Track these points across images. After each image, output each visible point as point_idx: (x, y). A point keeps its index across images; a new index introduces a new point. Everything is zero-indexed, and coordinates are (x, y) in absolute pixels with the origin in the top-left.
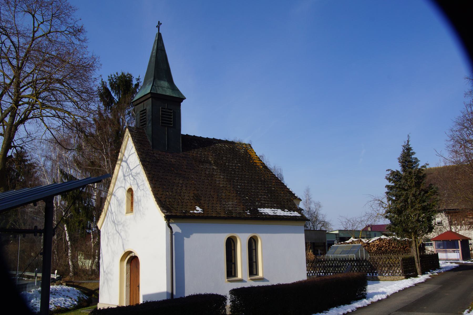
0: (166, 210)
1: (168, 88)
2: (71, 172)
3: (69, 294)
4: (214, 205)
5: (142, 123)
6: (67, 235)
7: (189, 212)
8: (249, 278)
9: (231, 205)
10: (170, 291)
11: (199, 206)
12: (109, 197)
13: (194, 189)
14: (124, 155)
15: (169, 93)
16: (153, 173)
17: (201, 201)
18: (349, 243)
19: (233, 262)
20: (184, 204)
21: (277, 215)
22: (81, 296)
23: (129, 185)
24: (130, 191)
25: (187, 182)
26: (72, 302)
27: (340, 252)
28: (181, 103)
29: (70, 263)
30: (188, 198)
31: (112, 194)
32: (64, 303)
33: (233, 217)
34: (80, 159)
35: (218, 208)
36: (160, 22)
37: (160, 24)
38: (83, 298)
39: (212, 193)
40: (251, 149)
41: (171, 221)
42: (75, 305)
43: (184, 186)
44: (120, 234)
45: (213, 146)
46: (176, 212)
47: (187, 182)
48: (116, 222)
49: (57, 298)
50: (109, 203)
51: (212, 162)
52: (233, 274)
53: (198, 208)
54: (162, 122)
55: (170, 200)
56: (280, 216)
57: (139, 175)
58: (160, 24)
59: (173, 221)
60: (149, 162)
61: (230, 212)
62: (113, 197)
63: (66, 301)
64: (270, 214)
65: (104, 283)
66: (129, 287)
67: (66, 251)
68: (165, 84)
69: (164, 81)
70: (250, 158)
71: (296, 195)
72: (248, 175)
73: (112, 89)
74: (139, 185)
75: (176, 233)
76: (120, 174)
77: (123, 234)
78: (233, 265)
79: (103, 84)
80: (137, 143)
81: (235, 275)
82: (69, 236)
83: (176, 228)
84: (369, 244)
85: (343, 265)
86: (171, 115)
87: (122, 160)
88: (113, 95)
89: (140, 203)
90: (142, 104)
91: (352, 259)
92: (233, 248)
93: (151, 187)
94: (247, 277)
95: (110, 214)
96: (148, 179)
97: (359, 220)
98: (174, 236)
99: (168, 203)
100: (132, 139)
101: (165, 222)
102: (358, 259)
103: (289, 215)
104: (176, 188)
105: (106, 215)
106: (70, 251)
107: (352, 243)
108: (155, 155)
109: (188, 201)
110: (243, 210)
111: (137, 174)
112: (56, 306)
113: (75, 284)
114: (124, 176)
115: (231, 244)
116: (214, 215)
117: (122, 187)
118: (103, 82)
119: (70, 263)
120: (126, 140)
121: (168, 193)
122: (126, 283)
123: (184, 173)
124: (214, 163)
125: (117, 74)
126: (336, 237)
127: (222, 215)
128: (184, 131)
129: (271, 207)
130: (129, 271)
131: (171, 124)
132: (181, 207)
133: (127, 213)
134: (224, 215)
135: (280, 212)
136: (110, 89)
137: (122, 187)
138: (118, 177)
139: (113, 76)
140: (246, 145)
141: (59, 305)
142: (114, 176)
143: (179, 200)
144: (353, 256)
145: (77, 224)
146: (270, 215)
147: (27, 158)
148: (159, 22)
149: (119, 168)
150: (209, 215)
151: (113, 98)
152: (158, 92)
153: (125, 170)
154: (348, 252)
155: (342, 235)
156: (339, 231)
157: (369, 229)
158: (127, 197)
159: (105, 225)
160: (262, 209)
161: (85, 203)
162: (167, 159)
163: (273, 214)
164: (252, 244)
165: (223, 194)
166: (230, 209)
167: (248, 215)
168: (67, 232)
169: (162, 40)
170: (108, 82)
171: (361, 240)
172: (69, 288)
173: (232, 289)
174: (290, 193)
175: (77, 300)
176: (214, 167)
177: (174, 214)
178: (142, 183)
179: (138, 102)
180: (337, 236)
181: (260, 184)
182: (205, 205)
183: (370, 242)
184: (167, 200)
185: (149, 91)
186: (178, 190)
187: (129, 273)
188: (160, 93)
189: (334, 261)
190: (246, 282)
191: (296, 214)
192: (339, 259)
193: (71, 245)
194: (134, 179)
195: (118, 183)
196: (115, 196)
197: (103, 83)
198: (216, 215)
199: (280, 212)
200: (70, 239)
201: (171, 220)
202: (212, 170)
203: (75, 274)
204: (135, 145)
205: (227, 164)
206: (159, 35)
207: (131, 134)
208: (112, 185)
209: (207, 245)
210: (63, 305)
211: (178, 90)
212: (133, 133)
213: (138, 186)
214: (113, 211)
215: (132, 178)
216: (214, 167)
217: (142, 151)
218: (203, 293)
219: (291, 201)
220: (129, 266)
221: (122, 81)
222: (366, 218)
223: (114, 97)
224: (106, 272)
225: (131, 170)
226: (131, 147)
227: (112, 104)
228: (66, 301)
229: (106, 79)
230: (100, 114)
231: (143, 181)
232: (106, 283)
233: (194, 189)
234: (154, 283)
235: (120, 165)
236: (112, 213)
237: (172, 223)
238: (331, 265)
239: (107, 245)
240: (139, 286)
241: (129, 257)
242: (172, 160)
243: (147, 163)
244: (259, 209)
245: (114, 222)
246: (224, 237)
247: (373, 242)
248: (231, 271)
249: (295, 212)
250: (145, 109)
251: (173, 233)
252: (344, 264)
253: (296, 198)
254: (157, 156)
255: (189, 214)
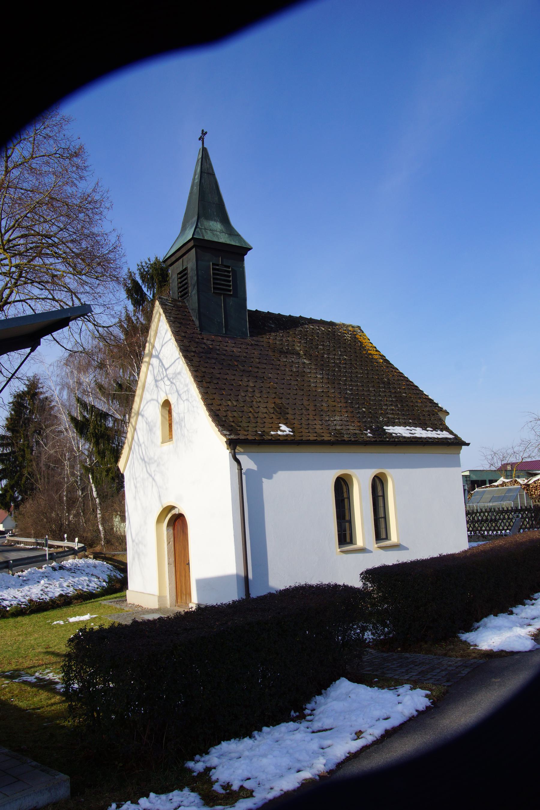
0: (229, 431)
1: (221, 232)
2: (89, 400)
3: (95, 572)
4: (310, 422)
5: (181, 292)
6: (94, 489)
7: (268, 434)
8: (376, 546)
9: (337, 421)
10: (242, 574)
11: (285, 424)
12: (135, 418)
13: (274, 395)
14: (153, 347)
15: (224, 239)
16: (204, 370)
17: (288, 416)
18: (497, 486)
19: (347, 518)
20: (259, 420)
21: (416, 438)
22: (113, 573)
23: (165, 395)
24: (167, 404)
25: (262, 385)
26: (99, 583)
27: (489, 500)
28: (245, 257)
29: (101, 528)
30: (265, 410)
31: (138, 414)
32: (88, 585)
33: (344, 440)
34: (103, 381)
35: (318, 427)
36: (205, 131)
37: (204, 133)
38: (114, 576)
39: (306, 403)
40: (361, 334)
41: (239, 449)
42: (103, 587)
43: (257, 391)
44: (153, 479)
45: (300, 329)
46: (246, 433)
47: (262, 385)
48: (146, 459)
49: (78, 577)
50: (135, 429)
51: (301, 352)
52: (348, 540)
53: (283, 427)
54: (214, 288)
55: (235, 414)
56: (421, 438)
57: (179, 376)
58: (204, 133)
59: (242, 450)
60: (195, 352)
61: (339, 433)
62: (140, 418)
63: (90, 581)
64: (404, 435)
65: (134, 559)
66: (173, 565)
67: (94, 511)
68: (217, 226)
69: (216, 221)
70: (362, 347)
71: (440, 405)
72: (361, 373)
73: (143, 281)
74: (181, 392)
75: (248, 470)
76: (150, 379)
77: (158, 478)
78: (347, 524)
79: (131, 276)
80: (174, 322)
81: (352, 541)
82: (96, 491)
83: (247, 462)
84: (528, 485)
85: (504, 518)
86: (229, 277)
87: (151, 355)
88: (145, 290)
89: (183, 424)
90: (181, 261)
91: (505, 509)
92: (345, 495)
93: (200, 392)
94: (372, 544)
95: (136, 447)
96: (195, 380)
97: (510, 451)
98: (244, 477)
99: (231, 419)
100: (166, 316)
101: (228, 451)
102: (524, 508)
103: (436, 436)
104: (243, 394)
105: (130, 448)
106: (99, 512)
107: (502, 485)
108: (205, 341)
109: (265, 415)
110: (360, 430)
111: (177, 374)
112: (76, 590)
113: (107, 556)
114: (156, 381)
115: (342, 488)
116: (312, 438)
117: (153, 400)
118: (130, 273)
119: (101, 528)
120: (156, 320)
121: (229, 403)
122: (169, 559)
123: (256, 370)
124: (305, 355)
125: (149, 260)
126: (467, 481)
127: (326, 438)
128: (251, 306)
129: (405, 424)
130: (172, 539)
131: (230, 291)
132: (254, 425)
133: (162, 443)
134: (329, 438)
135: (419, 433)
136: (140, 282)
137: (153, 400)
138: (146, 386)
139: (144, 264)
140: (353, 327)
141: (80, 587)
142: (140, 384)
143: (250, 415)
144: (507, 504)
145: (104, 473)
146: (405, 437)
147: (41, 390)
148: (203, 131)
149: (148, 369)
150: (304, 438)
151: (146, 294)
152: (206, 238)
153: (156, 371)
154: (502, 499)
155: (474, 478)
156: (470, 471)
157: (509, 468)
158: (162, 416)
159: (129, 465)
160: (390, 428)
161: (113, 443)
162: (226, 348)
163: (409, 435)
164: (378, 486)
165: (324, 404)
166: (338, 427)
167: (369, 437)
168: (93, 485)
169: (209, 159)
170: (137, 273)
171: (516, 481)
172: (97, 562)
173: (364, 569)
174: (431, 401)
175: (107, 580)
176: (305, 361)
177: (242, 437)
178: (186, 389)
179: (173, 259)
180: (468, 479)
181: (382, 387)
182: (295, 421)
183: (530, 482)
184: (229, 414)
185: (190, 237)
186: (247, 398)
187: (172, 543)
188: (210, 239)
189: (480, 513)
190: (371, 552)
191: (445, 434)
192: (497, 509)
193: (100, 504)
194: (172, 383)
195: (147, 396)
196: (143, 416)
197: (131, 275)
198: (315, 438)
199: (419, 433)
200: (97, 494)
201: (238, 448)
202: (301, 366)
203: (108, 542)
204: (170, 326)
205: (325, 356)
206: (204, 151)
207: (162, 308)
208: (137, 399)
209: (301, 489)
210: (86, 587)
211: (238, 235)
212: (167, 307)
213: (179, 395)
214: (141, 441)
215: (168, 383)
216: (305, 361)
217: (183, 334)
218: (314, 582)
219: (435, 414)
220: (172, 531)
221: (156, 270)
222: (521, 449)
223: (146, 293)
224: (136, 541)
225: (166, 370)
226: (165, 331)
227: (144, 302)
228: (90, 581)
229: (134, 269)
230: (128, 318)
231: (187, 385)
232: (136, 559)
233: (274, 395)
234: (216, 560)
235: (149, 364)
236: (139, 445)
237: (241, 453)
238: (493, 518)
239: (135, 498)
240: (188, 564)
241: (169, 516)
242: (235, 350)
243: (193, 354)
244: (385, 427)
245: (143, 460)
246: (330, 477)
247: (535, 482)
248: (345, 535)
249: (444, 432)
250: (186, 269)
251: (243, 471)
252: (506, 517)
253: (441, 409)
254: (209, 342)
255: (270, 438)
